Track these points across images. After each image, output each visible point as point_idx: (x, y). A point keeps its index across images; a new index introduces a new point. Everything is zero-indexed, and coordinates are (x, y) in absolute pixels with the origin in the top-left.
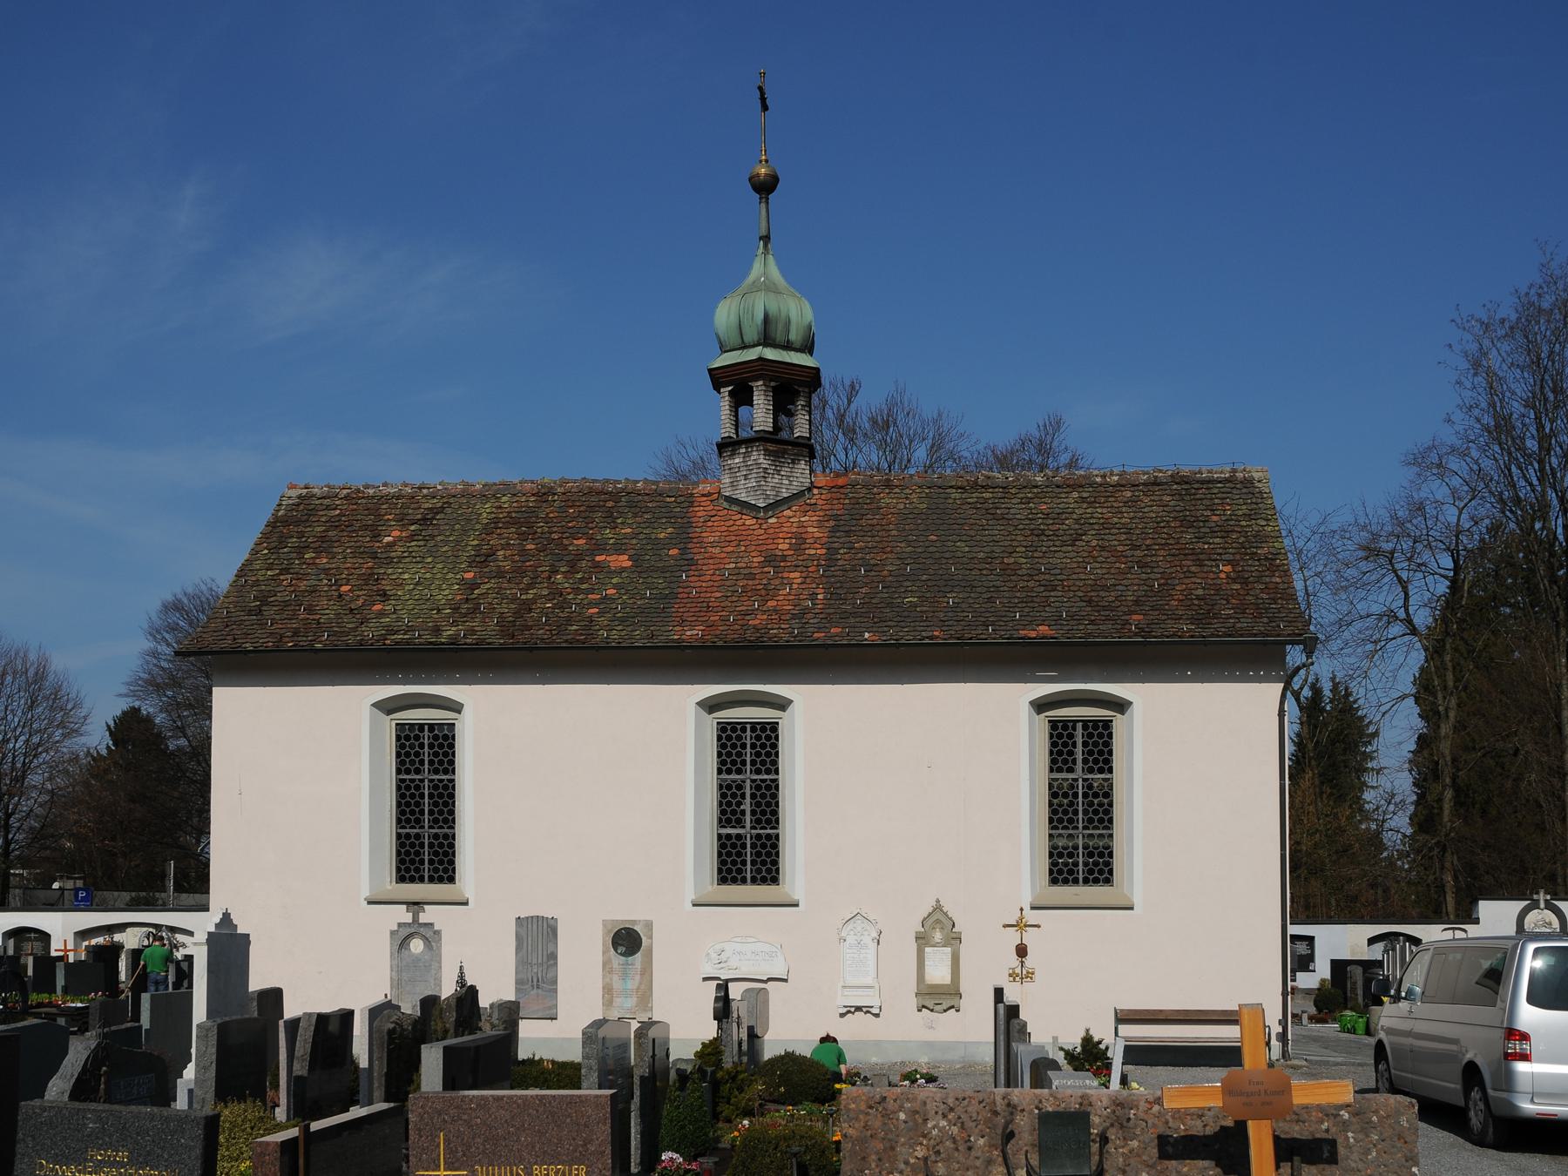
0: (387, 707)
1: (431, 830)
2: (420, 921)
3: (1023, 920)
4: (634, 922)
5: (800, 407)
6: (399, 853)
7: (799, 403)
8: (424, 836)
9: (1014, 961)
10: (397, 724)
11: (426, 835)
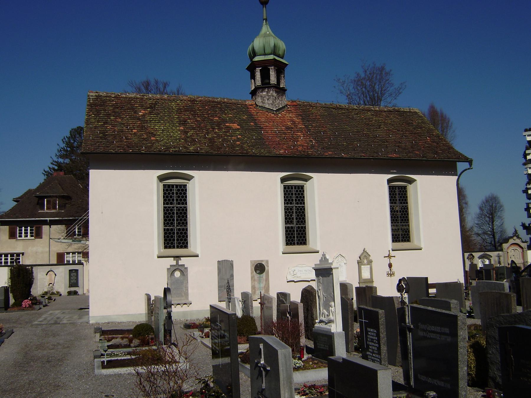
0: (161, 179)
1: (177, 227)
2: (179, 264)
3: (390, 255)
4: (262, 261)
5: (283, 77)
6: (305, 234)
7: (282, 76)
8: (175, 229)
9: (388, 269)
10: (163, 185)
11: (176, 229)
